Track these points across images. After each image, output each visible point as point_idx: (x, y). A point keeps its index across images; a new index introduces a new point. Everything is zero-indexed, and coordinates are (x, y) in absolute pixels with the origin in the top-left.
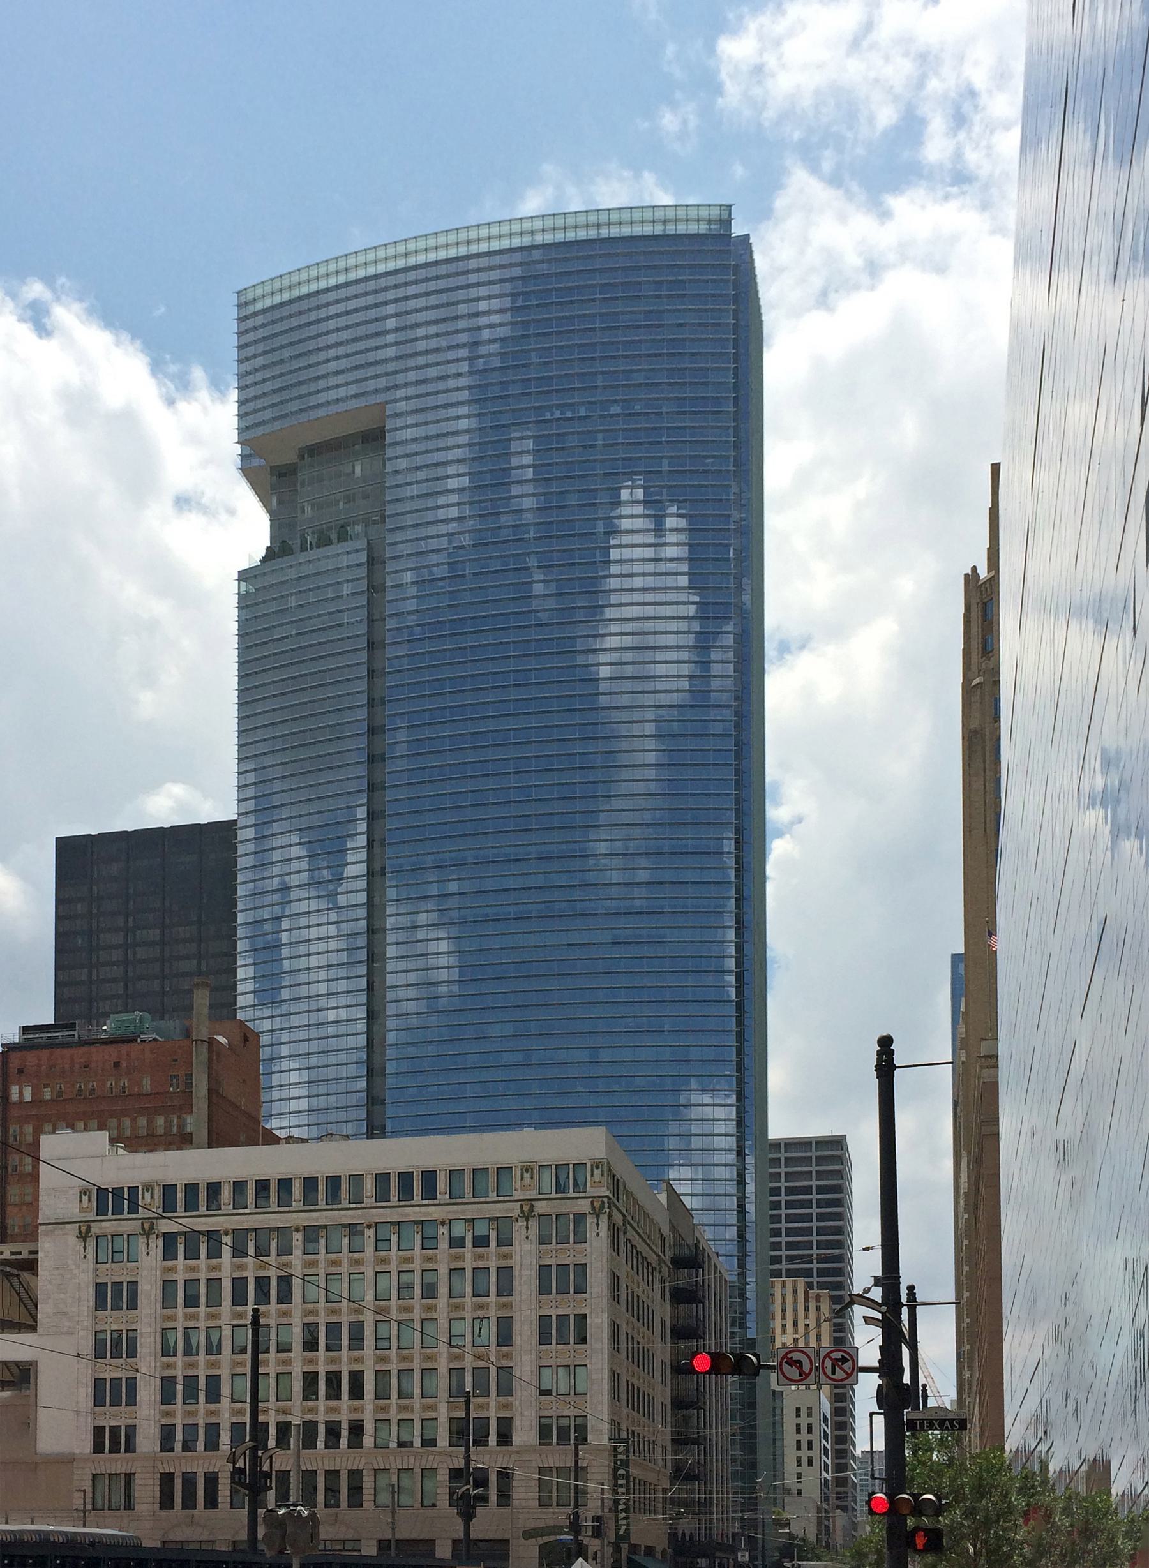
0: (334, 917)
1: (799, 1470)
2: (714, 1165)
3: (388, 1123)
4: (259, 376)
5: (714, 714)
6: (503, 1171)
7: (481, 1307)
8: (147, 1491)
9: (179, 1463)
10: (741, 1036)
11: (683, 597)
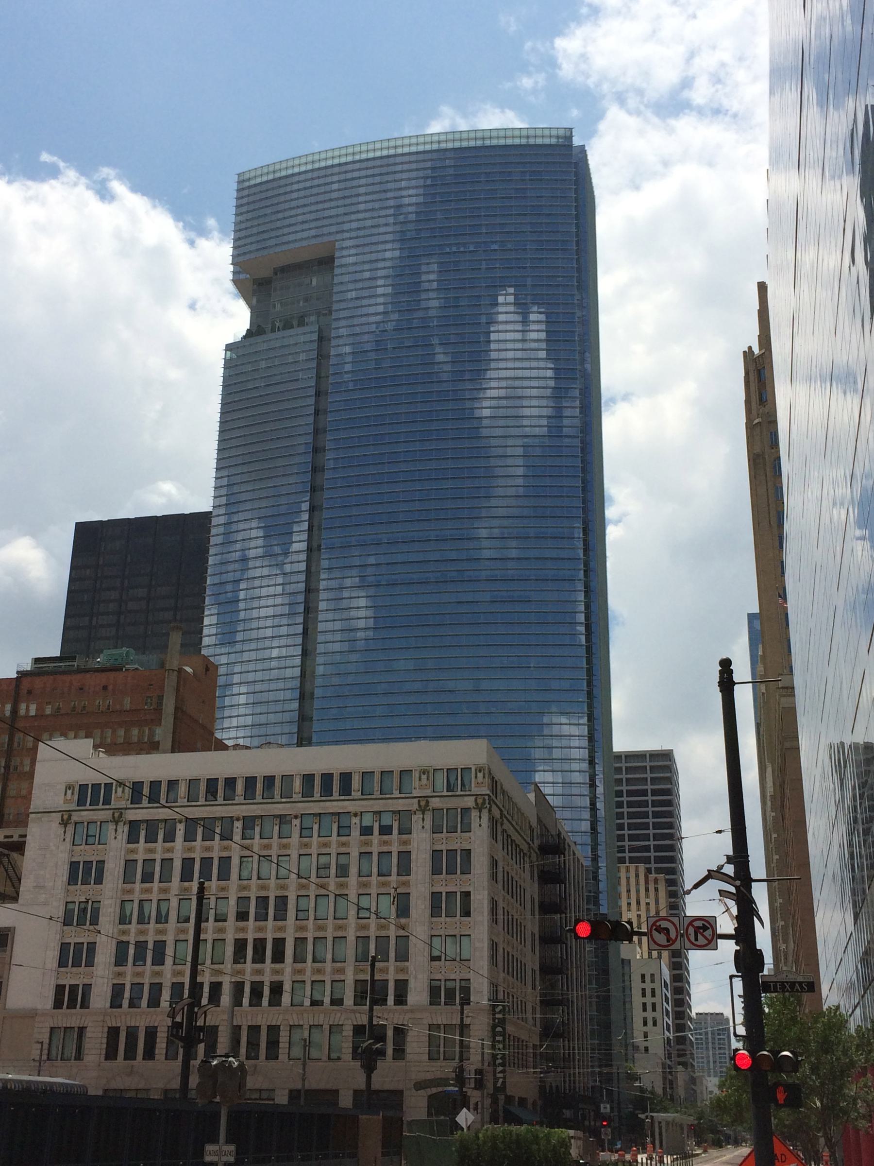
0: (280, 580)
6: (405, 773)
8: (95, 1041)
9: (125, 1018)
10: (590, 672)
11: (542, 364)
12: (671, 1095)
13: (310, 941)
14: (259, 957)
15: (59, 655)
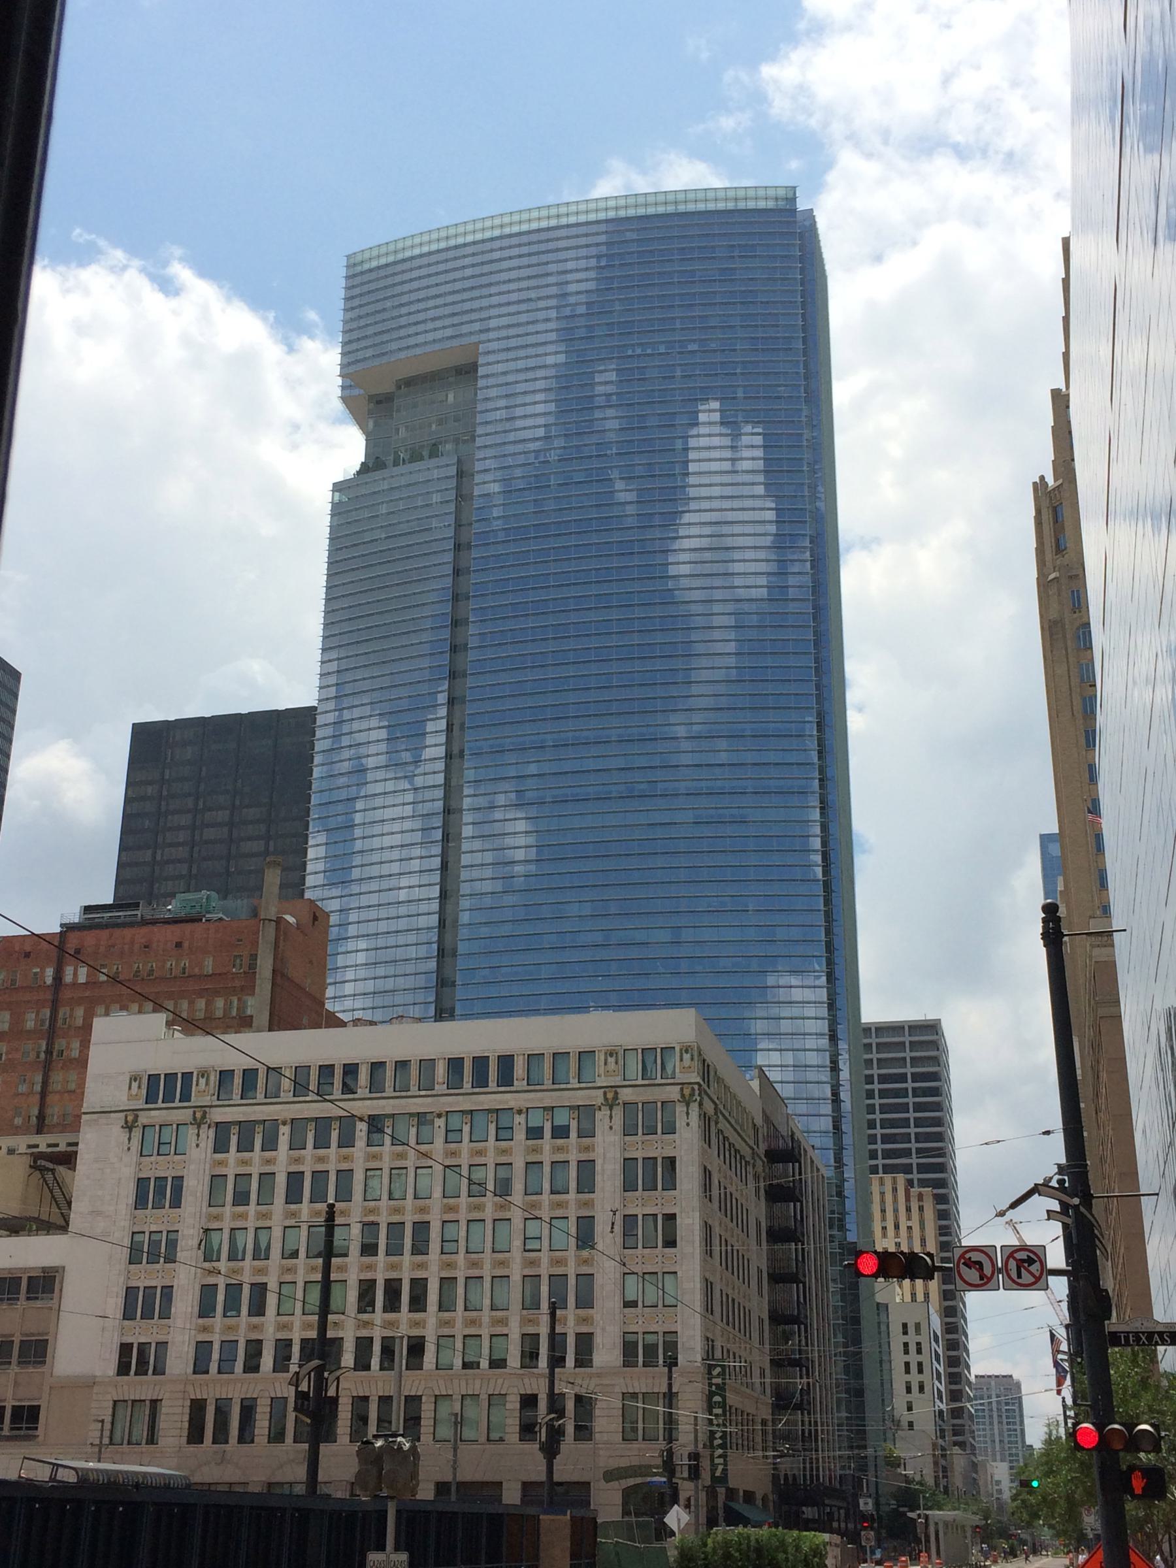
0: (409, 797)
1: (909, 1398)
2: (805, 1050)
3: (458, 1006)
4: (362, 322)
5: (792, 607)
6: (585, 1056)
7: (559, 1205)
8: (174, 1421)
9: (213, 1388)
10: (829, 916)
11: (758, 503)
12: (946, 1488)
13: (461, 1282)
14: (392, 1304)
15: (111, 902)
